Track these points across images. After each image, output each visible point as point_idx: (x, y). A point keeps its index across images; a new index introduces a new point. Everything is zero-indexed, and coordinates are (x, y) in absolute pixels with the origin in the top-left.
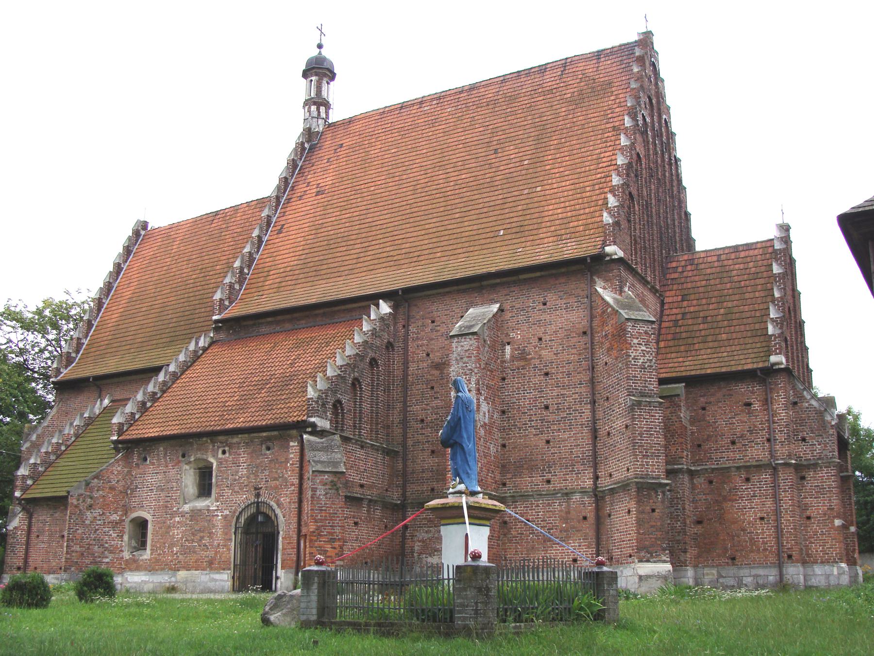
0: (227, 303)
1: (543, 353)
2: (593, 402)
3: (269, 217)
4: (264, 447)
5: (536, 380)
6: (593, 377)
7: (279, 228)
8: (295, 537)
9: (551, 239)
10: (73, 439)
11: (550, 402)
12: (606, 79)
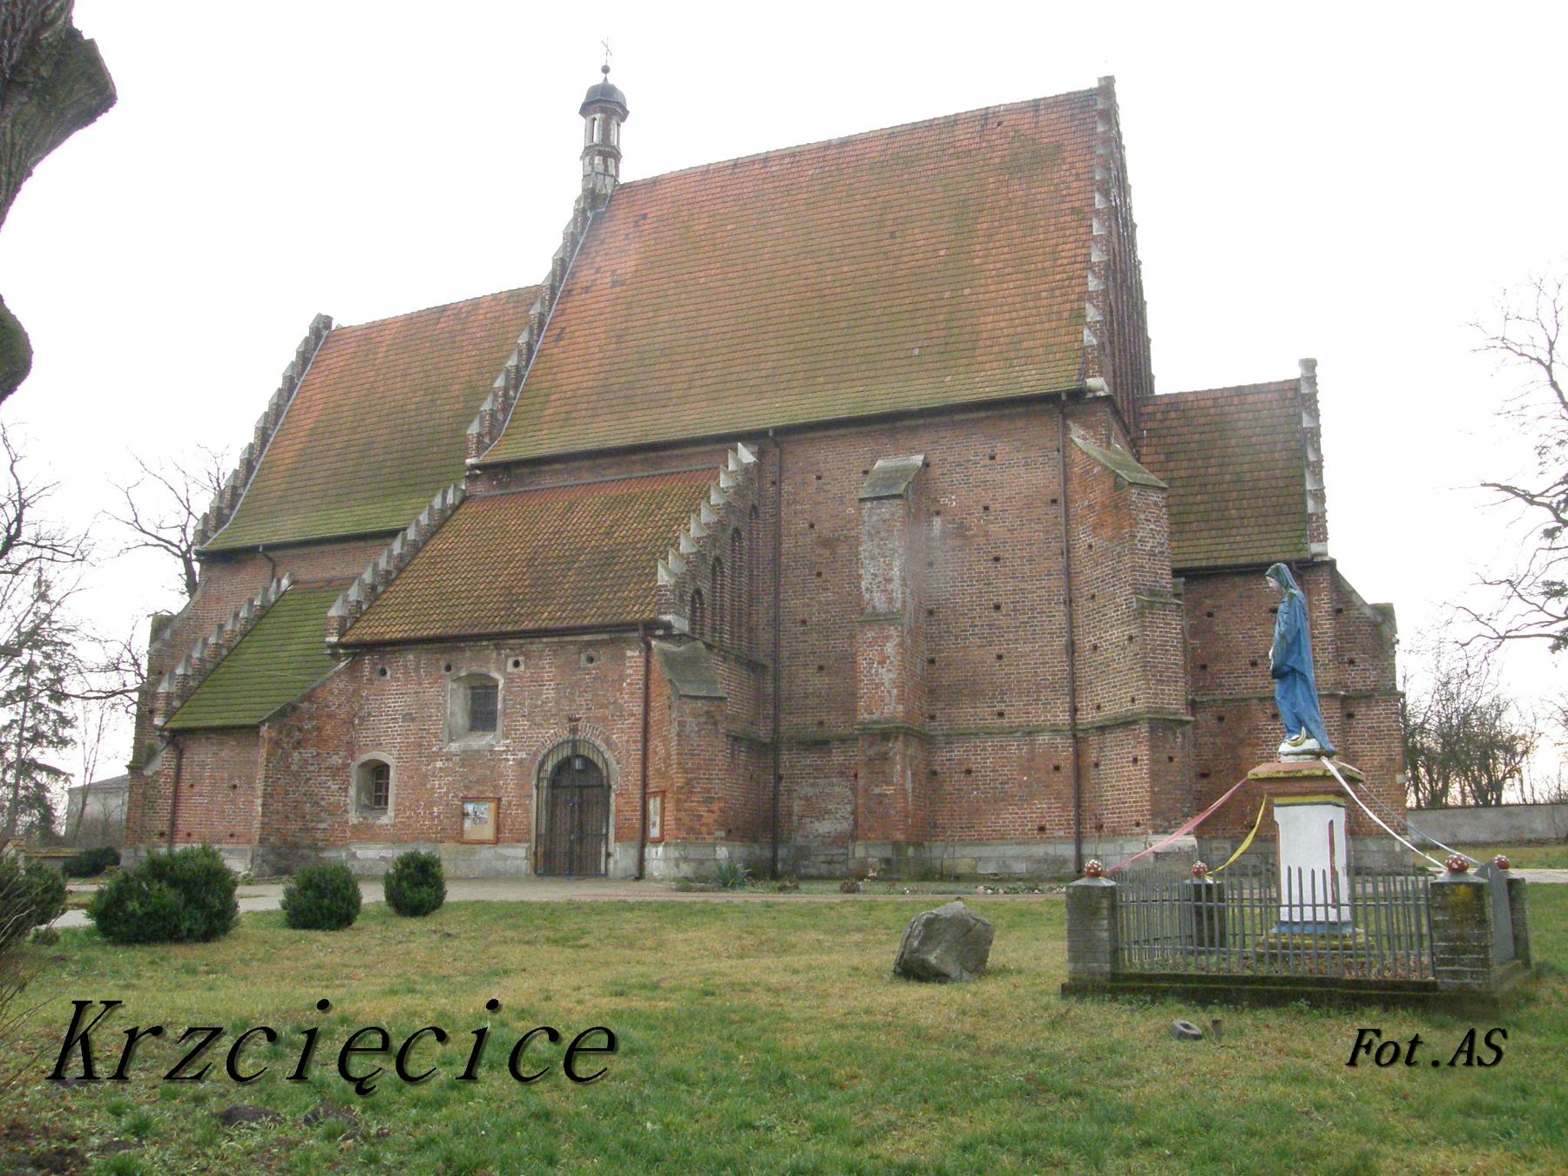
0: (487, 440)
2: (1069, 602)
3: (542, 316)
4: (583, 657)
6: (1069, 566)
7: (558, 331)
8: (637, 794)
9: (995, 365)
10: (239, 638)
11: (1002, 600)
12: (1053, 139)
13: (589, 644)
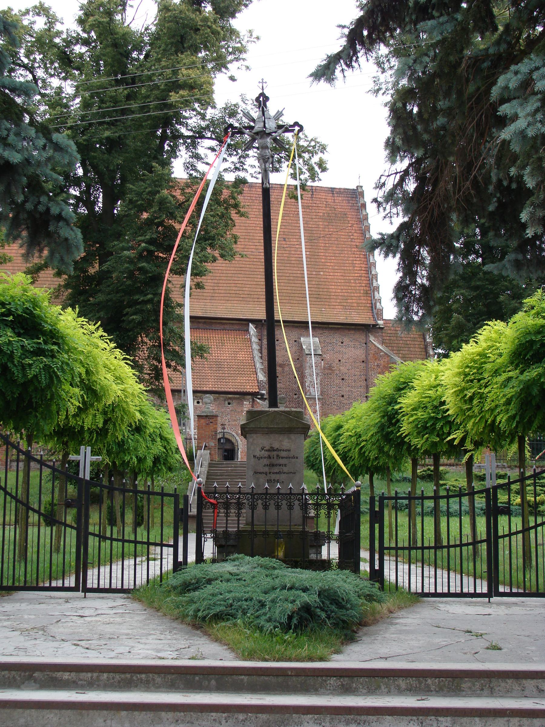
1: (341, 368)
4: (227, 402)
5: (337, 381)
11: (344, 394)
13: (230, 398)
